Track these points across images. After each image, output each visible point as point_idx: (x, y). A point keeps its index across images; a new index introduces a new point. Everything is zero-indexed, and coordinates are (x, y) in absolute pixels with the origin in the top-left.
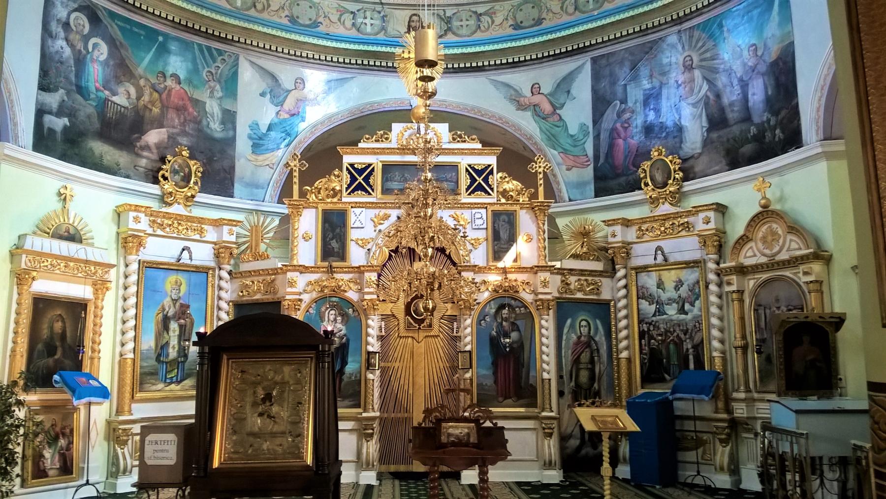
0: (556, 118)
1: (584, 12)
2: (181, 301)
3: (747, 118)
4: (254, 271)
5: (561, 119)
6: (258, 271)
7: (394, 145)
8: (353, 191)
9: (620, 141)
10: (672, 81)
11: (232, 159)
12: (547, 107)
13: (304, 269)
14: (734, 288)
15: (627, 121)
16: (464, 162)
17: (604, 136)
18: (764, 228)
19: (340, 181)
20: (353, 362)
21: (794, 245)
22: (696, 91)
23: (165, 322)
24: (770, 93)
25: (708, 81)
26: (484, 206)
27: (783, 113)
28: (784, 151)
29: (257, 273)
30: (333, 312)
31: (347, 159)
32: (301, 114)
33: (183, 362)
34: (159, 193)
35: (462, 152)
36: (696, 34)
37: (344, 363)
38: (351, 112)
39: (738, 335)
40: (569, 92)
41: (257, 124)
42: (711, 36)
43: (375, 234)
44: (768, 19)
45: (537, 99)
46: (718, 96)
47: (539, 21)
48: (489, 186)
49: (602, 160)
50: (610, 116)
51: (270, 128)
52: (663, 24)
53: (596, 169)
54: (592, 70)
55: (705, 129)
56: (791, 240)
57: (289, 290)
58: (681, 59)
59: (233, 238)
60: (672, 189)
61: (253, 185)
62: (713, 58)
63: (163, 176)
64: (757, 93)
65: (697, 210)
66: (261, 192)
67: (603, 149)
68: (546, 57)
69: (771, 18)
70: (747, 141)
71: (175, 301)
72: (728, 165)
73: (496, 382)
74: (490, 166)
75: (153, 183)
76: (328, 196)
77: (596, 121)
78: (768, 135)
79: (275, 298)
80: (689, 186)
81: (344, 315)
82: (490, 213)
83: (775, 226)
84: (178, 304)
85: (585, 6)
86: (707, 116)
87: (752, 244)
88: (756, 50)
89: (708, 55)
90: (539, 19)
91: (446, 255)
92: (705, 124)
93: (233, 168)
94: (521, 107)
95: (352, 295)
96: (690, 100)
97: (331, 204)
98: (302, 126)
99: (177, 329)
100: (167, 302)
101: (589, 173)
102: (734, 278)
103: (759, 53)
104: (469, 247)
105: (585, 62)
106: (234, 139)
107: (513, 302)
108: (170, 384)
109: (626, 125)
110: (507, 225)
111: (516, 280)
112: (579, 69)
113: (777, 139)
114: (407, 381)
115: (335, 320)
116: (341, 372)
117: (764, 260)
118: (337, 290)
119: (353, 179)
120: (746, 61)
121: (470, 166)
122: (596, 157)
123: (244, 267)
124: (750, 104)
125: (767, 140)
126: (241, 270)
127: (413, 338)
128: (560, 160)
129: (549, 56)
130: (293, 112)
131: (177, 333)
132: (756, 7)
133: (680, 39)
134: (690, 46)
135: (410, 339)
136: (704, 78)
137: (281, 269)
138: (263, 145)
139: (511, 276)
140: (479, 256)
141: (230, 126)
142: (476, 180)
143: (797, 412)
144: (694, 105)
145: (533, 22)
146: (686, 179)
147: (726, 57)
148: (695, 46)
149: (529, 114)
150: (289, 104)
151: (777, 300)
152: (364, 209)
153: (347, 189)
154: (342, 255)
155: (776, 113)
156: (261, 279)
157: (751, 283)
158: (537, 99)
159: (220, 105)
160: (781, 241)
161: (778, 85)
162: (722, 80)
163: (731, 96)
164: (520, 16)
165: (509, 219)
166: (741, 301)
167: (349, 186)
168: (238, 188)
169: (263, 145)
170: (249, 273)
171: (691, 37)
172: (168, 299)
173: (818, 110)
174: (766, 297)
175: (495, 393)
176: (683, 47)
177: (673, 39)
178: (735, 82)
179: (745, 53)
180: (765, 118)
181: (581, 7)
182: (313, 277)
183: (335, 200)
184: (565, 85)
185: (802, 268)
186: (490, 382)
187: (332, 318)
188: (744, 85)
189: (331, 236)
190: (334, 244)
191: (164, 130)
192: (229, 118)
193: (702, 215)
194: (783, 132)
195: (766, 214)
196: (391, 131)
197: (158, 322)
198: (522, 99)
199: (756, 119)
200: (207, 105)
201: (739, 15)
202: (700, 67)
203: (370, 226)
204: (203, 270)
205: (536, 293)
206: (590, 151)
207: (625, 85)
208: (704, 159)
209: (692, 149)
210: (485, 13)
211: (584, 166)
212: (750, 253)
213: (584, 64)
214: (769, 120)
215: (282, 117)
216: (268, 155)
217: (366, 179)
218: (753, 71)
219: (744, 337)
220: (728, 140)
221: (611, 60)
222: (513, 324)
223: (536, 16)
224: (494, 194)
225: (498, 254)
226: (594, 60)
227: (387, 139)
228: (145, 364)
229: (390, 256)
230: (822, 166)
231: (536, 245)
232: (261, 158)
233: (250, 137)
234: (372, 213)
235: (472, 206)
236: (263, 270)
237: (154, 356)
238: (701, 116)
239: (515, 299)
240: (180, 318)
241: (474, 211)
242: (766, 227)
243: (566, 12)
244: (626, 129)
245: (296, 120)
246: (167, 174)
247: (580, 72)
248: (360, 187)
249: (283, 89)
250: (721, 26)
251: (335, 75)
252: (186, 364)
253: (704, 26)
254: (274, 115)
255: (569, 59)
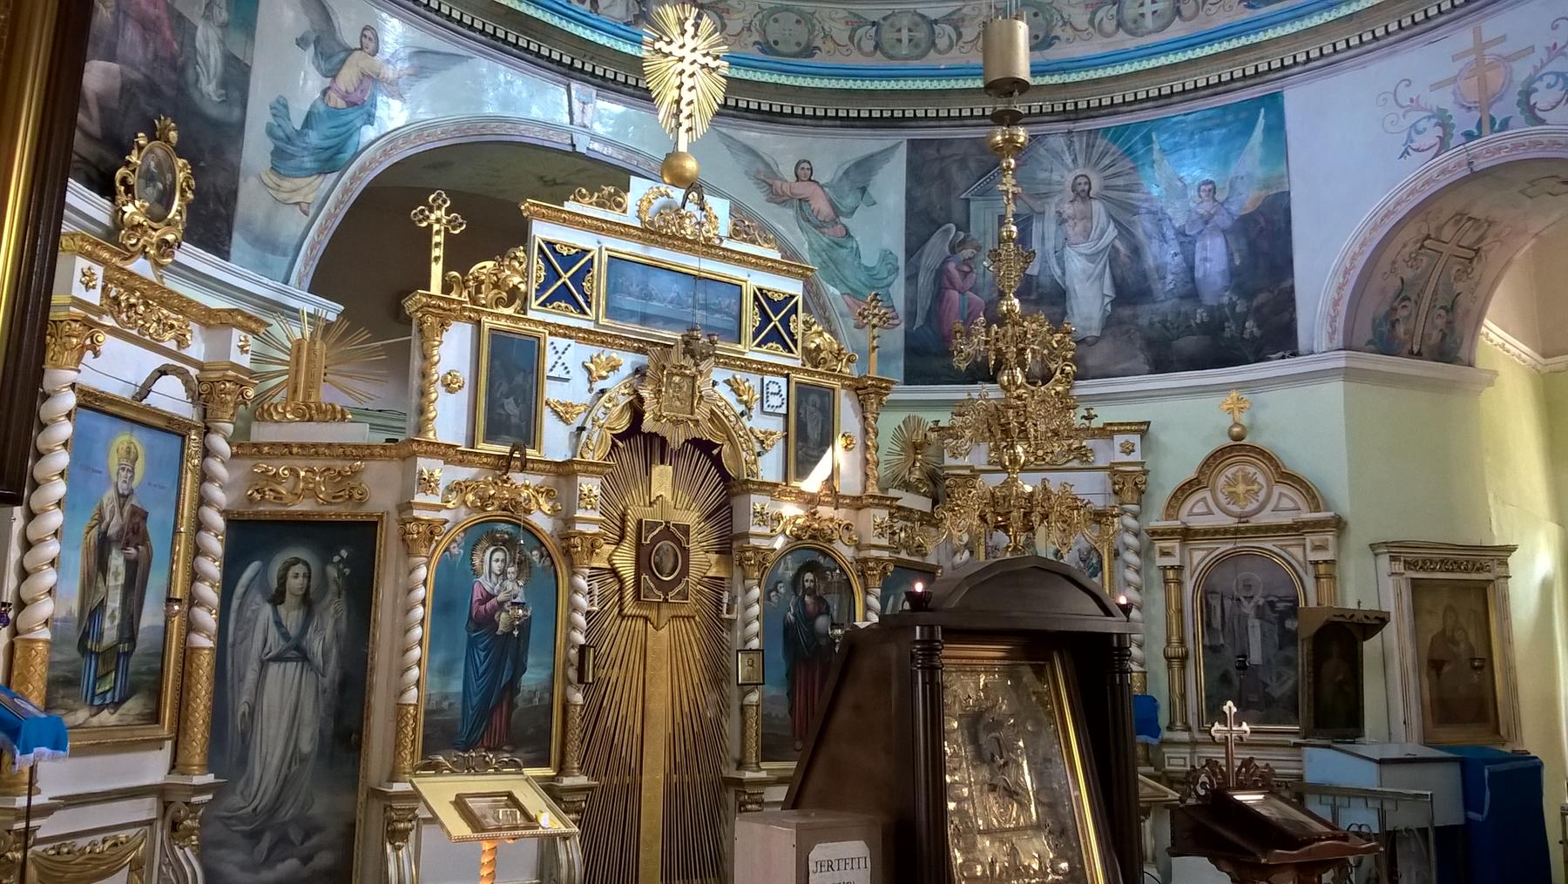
0: (839, 230)
1: (891, 57)
2: (134, 502)
3: (1191, 292)
4: (302, 446)
5: (848, 234)
6: (314, 445)
7: (630, 219)
8: (550, 300)
9: (955, 295)
10: (1051, 211)
11: (234, 173)
12: (821, 205)
13: (447, 453)
14: (1175, 561)
15: (966, 261)
16: (755, 280)
17: (924, 280)
18: (1230, 472)
19: (525, 271)
20: (538, 665)
21: (1286, 503)
22: (1094, 235)
23: (102, 548)
24: (1237, 262)
25: (1118, 224)
26: (779, 370)
27: (1261, 298)
28: (1260, 357)
29: (310, 450)
30: (499, 555)
31: (541, 231)
32: (367, 107)
33: (128, 654)
34: (105, 219)
35: (743, 260)
36: (1101, 143)
37: (520, 668)
38: (459, 126)
39: (1174, 639)
40: (864, 190)
41: (286, 107)
42: (1129, 152)
43: (590, 396)
44: (1242, 147)
45: (804, 189)
46: (1136, 251)
47: (809, 51)
48: (791, 335)
49: (919, 322)
50: (937, 246)
51: (307, 123)
52: (1047, 114)
53: (908, 335)
54: (909, 162)
55: (1107, 300)
56: (1281, 495)
57: (419, 498)
58: (1070, 178)
59: (245, 361)
60: (1059, 389)
61: (267, 244)
62: (1129, 189)
63: (124, 181)
64: (1214, 258)
65: (1107, 432)
66: (281, 263)
67: (924, 303)
68: (831, 118)
69: (1248, 148)
70: (1189, 331)
71: (123, 498)
72: (1148, 362)
73: (791, 711)
74: (792, 297)
75: (102, 195)
76: (498, 302)
77: (914, 247)
78: (1230, 329)
79: (361, 514)
80: (1084, 388)
81: (523, 565)
82: (793, 385)
83: (1251, 469)
84: (127, 508)
85: (893, 47)
86: (1114, 277)
87: (1206, 494)
88: (1214, 190)
89: (1120, 182)
90: (808, 46)
91: (710, 455)
92: (1108, 289)
93: (234, 194)
94: (777, 197)
95: (542, 520)
96: (1085, 248)
97: (500, 319)
98: (369, 133)
99: (122, 569)
100: (109, 498)
101: (895, 339)
102: (1174, 545)
103: (1220, 197)
104: (758, 448)
105: (896, 146)
106: (241, 126)
107: (821, 560)
108: (101, 708)
109: (966, 269)
110: (817, 414)
111: (832, 520)
112: (886, 154)
113: (1247, 336)
114: (631, 709)
115: (504, 573)
116: (513, 686)
117: (1230, 522)
118: (514, 508)
119: (553, 275)
120: (1192, 205)
121: (760, 290)
122: (911, 315)
123: (263, 433)
124: (1198, 274)
125: (1227, 334)
126: (254, 438)
127: (646, 619)
128: (845, 309)
129: (837, 117)
130: (353, 99)
131: (121, 580)
132: (1218, 126)
133: (1070, 145)
134: (1088, 158)
135: (641, 622)
136: (1110, 216)
137: (383, 447)
138: (293, 156)
139: (825, 511)
140: (769, 467)
141: (236, 94)
142: (771, 320)
143: (1381, 762)
144: (1091, 257)
145: (796, 49)
146: (1077, 377)
147: (1155, 191)
148: (1097, 164)
149: (790, 213)
150: (348, 77)
151: (1248, 587)
152: (572, 342)
153: (539, 292)
154: (527, 434)
155: (1249, 295)
156: (318, 465)
157: (1199, 556)
158: (804, 189)
159: (222, 42)
160: (1262, 496)
161: (1253, 251)
162: (1143, 226)
163: (1163, 256)
164: (774, 32)
165: (823, 402)
166: (1180, 583)
167: (542, 288)
168: (238, 241)
169: (293, 156)
170: (285, 449)
171: (1090, 146)
172: (111, 493)
173: (1336, 303)
174: (1229, 581)
175: (789, 733)
176: (1075, 160)
177: (1059, 142)
178: (1170, 234)
179: (1192, 193)
180: (1225, 300)
181: (886, 46)
182: (464, 473)
183: (510, 311)
184: (861, 173)
185: (1309, 539)
186: (781, 711)
187: (496, 567)
188: (1186, 241)
189: (504, 388)
190: (511, 407)
191: (115, 67)
192: (237, 76)
193: (1119, 439)
194: (1259, 327)
195: (1237, 448)
196: (627, 190)
197: (88, 548)
198: (778, 183)
199: (1209, 300)
200: (199, 34)
201: (1183, 130)
202: (1103, 198)
203: (580, 378)
204: (172, 427)
205: (858, 547)
206: (899, 303)
207: (968, 201)
208: (1105, 347)
209: (1084, 329)
210: (948, 19)
211: (886, 322)
212: (1200, 508)
213: (896, 146)
214: (1233, 305)
215: (332, 104)
216: (299, 182)
217: (577, 279)
218: (1206, 222)
219: (1182, 642)
220: (1151, 324)
221: (944, 152)
222: (820, 600)
223: (804, 40)
224: (798, 353)
225: (803, 462)
226: (913, 145)
227: (619, 205)
228: (58, 658)
229: (614, 445)
230: (1334, 390)
231: (859, 456)
232: (287, 184)
233: (270, 132)
234: (585, 352)
235: (762, 369)
236: (329, 446)
237: (75, 636)
238: (1101, 276)
239: (825, 554)
240: (128, 544)
241: (767, 379)
242: (1233, 469)
243: (860, 49)
244: (965, 274)
245: (354, 115)
246: (132, 180)
247: (888, 160)
248: (564, 294)
249: (339, 44)
250: (1147, 140)
251: (433, 42)
252: (133, 660)
253: (1117, 134)
254: (318, 95)
255: (869, 132)
